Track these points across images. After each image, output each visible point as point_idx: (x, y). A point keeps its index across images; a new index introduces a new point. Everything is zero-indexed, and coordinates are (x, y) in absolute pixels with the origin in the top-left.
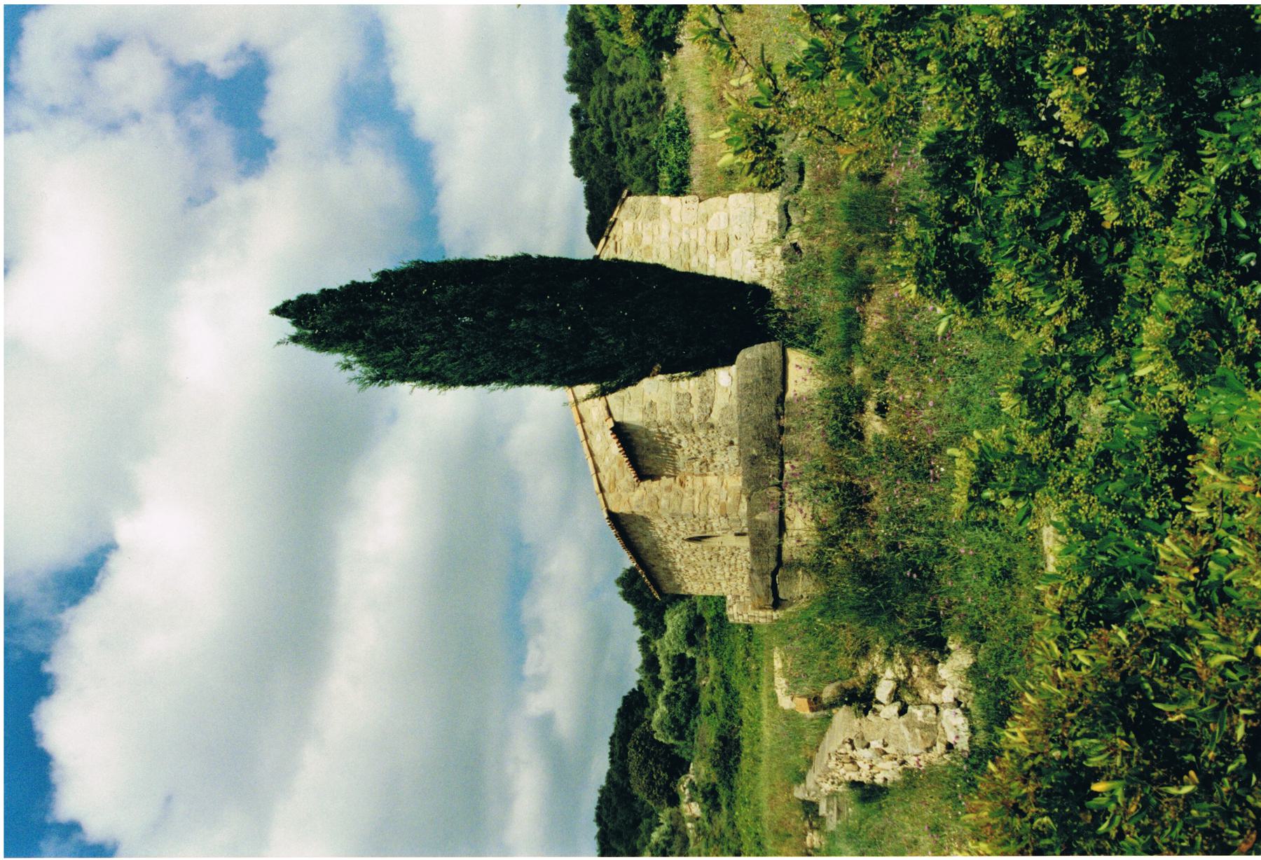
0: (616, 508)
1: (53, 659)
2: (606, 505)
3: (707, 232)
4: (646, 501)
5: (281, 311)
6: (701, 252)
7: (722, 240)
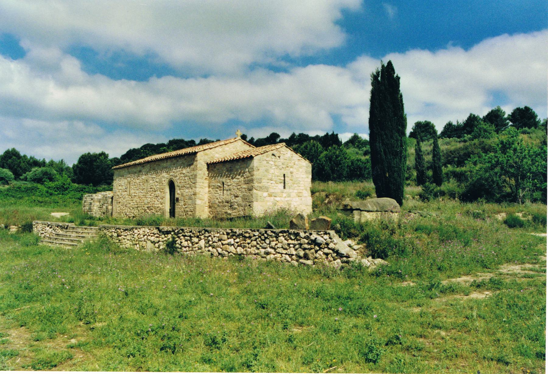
0: (198, 155)
2: (200, 151)
3: (303, 190)
6: (297, 188)
7: (301, 195)
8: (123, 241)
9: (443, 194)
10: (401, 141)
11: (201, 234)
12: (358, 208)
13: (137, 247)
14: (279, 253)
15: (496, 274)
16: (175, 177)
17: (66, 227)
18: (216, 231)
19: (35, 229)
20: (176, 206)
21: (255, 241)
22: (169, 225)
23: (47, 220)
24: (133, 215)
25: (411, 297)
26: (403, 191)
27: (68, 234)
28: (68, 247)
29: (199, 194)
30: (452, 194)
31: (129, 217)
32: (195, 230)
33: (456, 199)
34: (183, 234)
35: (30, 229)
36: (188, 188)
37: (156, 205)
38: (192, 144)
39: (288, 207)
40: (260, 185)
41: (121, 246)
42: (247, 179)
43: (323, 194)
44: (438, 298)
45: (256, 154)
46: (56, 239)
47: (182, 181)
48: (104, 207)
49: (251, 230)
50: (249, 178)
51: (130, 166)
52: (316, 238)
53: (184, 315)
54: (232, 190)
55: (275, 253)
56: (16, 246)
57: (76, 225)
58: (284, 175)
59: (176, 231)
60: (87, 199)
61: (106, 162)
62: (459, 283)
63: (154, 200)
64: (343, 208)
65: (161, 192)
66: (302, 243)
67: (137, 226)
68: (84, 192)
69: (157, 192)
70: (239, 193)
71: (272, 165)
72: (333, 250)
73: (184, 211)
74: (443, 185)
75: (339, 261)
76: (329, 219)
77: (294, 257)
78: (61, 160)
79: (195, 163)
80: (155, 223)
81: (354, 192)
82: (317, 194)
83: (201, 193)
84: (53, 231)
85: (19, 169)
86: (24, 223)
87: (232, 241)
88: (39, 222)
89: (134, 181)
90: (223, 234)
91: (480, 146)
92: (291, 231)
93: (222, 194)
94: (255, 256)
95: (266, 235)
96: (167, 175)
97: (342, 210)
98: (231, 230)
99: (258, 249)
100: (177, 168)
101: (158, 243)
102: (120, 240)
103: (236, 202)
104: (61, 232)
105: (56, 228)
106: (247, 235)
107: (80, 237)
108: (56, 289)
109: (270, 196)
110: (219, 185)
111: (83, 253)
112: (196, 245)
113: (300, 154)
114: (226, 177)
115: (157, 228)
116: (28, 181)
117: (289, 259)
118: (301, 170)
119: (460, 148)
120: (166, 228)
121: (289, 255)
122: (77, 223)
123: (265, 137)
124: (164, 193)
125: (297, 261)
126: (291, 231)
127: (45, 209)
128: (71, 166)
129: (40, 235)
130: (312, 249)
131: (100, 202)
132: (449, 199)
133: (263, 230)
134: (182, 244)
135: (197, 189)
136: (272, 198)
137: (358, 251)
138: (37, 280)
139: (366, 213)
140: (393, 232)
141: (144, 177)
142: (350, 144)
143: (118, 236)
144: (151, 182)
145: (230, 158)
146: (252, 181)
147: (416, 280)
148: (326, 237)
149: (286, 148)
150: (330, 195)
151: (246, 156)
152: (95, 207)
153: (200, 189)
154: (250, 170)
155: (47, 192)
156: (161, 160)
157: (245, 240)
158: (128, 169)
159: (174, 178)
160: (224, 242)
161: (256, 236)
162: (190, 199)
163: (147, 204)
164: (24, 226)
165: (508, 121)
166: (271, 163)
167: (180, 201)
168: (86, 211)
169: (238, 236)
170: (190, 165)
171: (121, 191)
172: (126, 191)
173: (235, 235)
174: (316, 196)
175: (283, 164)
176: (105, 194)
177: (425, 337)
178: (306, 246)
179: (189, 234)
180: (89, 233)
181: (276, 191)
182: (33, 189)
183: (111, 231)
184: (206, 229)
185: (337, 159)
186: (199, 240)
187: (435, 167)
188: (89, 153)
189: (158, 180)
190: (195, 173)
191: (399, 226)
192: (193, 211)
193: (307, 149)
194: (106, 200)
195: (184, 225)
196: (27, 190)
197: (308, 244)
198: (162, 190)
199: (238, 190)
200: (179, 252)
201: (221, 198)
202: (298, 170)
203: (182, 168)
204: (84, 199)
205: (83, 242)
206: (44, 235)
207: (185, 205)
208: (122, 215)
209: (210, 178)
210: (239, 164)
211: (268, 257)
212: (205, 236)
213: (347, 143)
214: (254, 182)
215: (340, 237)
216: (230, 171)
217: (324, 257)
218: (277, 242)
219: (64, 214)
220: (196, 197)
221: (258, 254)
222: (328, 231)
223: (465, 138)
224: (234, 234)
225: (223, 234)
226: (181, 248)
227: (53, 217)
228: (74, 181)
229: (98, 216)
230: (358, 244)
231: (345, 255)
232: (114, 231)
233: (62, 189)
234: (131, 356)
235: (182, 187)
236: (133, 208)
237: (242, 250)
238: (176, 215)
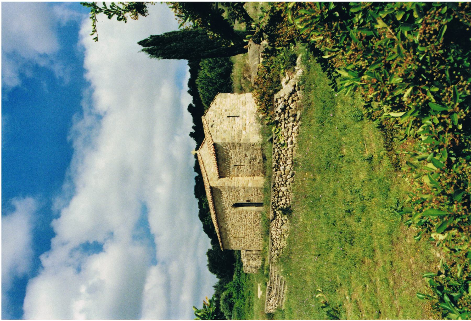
0: (212, 185)
1: (62, 217)
4: (221, 183)
6: (238, 105)
7: (244, 102)
8: (281, 246)
10: (202, 34)
14: (291, 134)
17: (270, 288)
19: (272, 311)
20: (254, 202)
22: (269, 212)
23: (265, 302)
24: (260, 235)
27: (275, 287)
28: (286, 288)
32: (273, 194)
36: (239, 193)
39: (254, 114)
40: (236, 137)
42: (232, 148)
46: (279, 296)
47: (233, 197)
48: (254, 256)
49: (273, 154)
50: (231, 146)
51: (221, 238)
52: (280, 109)
53: (333, 223)
54: (241, 158)
55: (291, 137)
57: (268, 281)
58: (228, 117)
59: (274, 208)
65: (242, 213)
67: (270, 236)
68: (241, 270)
70: (244, 152)
72: (289, 97)
73: (257, 195)
77: (294, 124)
78: (214, 288)
79: (219, 188)
80: (268, 223)
82: (243, 85)
87: (282, 168)
88: (266, 308)
89: (233, 234)
90: (276, 174)
94: (294, 151)
96: (229, 209)
98: (273, 168)
99: (288, 149)
100: (222, 202)
101: (283, 221)
102: (281, 248)
103: (250, 155)
105: (271, 295)
106: (277, 157)
107: (278, 278)
108: (316, 303)
109: (245, 129)
110: (236, 168)
111: (291, 278)
112: (285, 193)
117: (296, 127)
118: (224, 103)
120: (271, 215)
121: (293, 127)
122: (267, 280)
123: (191, 117)
125: (298, 122)
127: (255, 303)
128: (218, 280)
131: (249, 260)
133: (274, 146)
136: (247, 127)
137: (291, 77)
138: (310, 314)
141: (230, 227)
143: (277, 249)
144: (234, 221)
146: (233, 144)
148: (279, 101)
152: (254, 263)
153: (240, 184)
154: (225, 145)
155: (241, 299)
156: (216, 214)
157: (282, 158)
158: (223, 239)
159: (231, 204)
160: (283, 173)
162: (247, 191)
167: (249, 199)
168: (256, 271)
169: (278, 163)
170: (220, 191)
171: (241, 244)
174: (245, 86)
175: (219, 118)
176: (243, 255)
178: (286, 115)
179: (276, 198)
181: (241, 123)
182: (239, 311)
183: (273, 255)
184: (272, 186)
185: (212, 62)
186: (281, 191)
188: (208, 265)
189: (232, 216)
190: (227, 188)
192: (257, 189)
193: (204, 87)
194: (248, 255)
197: (285, 114)
198: (241, 213)
199: (241, 154)
200: (290, 206)
202: (224, 105)
204: (247, 272)
205: (282, 277)
208: (260, 243)
211: (294, 142)
212: (278, 187)
214: (234, 142)
215: (279, 90)
216: (225, 160)
217: (294, 103)
221: (292, 149)
222: (275, 100)
224: (276, 166)
225: (276, 174)
227: (262, 297)
231: (293, 88)
232: (273, 253)
233: (239, 287)
234: (356, 265)
237: (289, 160)
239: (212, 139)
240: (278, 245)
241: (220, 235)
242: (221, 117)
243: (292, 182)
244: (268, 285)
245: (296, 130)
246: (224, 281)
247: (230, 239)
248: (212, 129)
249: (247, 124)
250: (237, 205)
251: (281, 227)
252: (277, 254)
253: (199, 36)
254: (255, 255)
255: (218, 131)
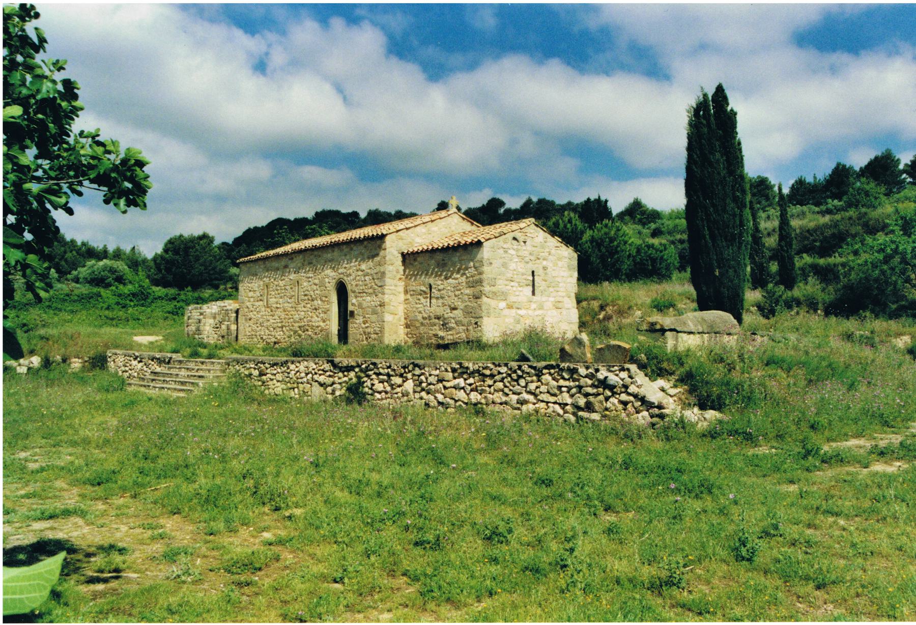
0: (388, 238)
3: (563, 297)
5: (720, 90)
7: (560, 305)
8: (270, 383)
9: (799, 303)
11: (407, 370)
12: (673, 327)
13: (294, 394)
14: (542, 401)
15: (907, 436)
16: (347, 276)
17: (167, 360)
18: (432, 365)
19: (111, 365)
20: (350, 325)
21: (500, 381)
23: (131, 349)
24: (274, 340)
25: (777, 469)
26: (742, 300)
27: (172, 371)
29: (389, 304)
30: (812, 303)
31: (268, 343)
32: (397, 364)
33: (819, 312)
34: (376, 370)
35: (103, 365)
36: (370, 294)
37: (314, 324)
38: (376, 218)
40: (493, 289)
41: (267, 392)
42: (471, 279)
43: (595, 305)
44: (819, 471)
45: (487, 238)
46: (153, 380)
47: (361, 283)
48: (224, 327)
49: (494, 364)
50: (474, 278)
51: (267, 258)
52: (606, 378)
54: (447, 298)
55: (535, 401)
56: (89, 391)
57: (184, 356)
58: (533, 272)
59: (363, 366)
60: (193, 314)
61: (211, 250)
62: (850, 449)
63: (310, 314)
64: (648, 328)
66: (581, 384)
69: (315, 301)
70: (459, 304)
71: (512, 255)
72: (635, 396)
74: (796, 288)
75: (645, 413)
76: (627, 346)
77: (568, 408)
79: (382, 253)
80: (323, 353)
81: (648, 301)
82: (584, 304)
83: (392, 304)
84: (145, 367)
85: (63, 263)
86: (92, 353)
87: (461, 382)
88: (118, 352)
90: (446, 370)
91: (861, 222)
92: (562, 365)
93: (428, 304)
95: (519, 372)
96: (334, 273)
97: (647, 331)
98: (460, 364)
99: (507, 395)
101: (331, 385)
102: (264, 382)
103: (454, 318)
104: (158, 369)
105: (150, 362)
106: (488, 372)
107: (195, 376)
109: (510, 307)
110: (424, 289)
112: (399, 390)
113: (559, 237)
114: (436, 276)
115: (328, 362)
116: (80, 283)
118: (560, 264)
119: (825, 226)
121: (560, 404)
122: (185, 354)
123: (479, 205)
124: (329, 302)
125: (574, 414)
126: (562, 365)
129: (120, 373)
130: (599, 394)
131: (215, 318)
132: (808, 312)
133: (514, 365)
134: (374, 388)
135: (386, 296)
136: (513, 311)
139: (684, 336)
140: (731, 368)
141: (292, 276)
142: (627, 218)
143: (262, 374)
144: (305, 284)
145: (441, 245)
146: (480, 282)
147: (775, 444)
148: (624, 375)
149: (536, 228)
150: (607, 305)
151: (470, 241)
154: (477, 265)
156: (323, 248)
157: (484, 381)
158: (264, 263)
159: (345, 278)
160: (448, 384)
161: (502, 373)
162: (374, 312)
163: (298, 322)
164: (93, 359)
165: (904, 176)
166: (511, 252)
167: (356, 317)
168: (191, 333)
169: (472, 374)
170: (373, 257)
171: (252, 300)
172: (261, 300)
173: (467, 372)
175: (530, 254)
177: (815, 527)
178: (590, 390)
179: (386, 371)
180: (209, 371)
181: (520, 299)
182: (92, 297)
183: (248, 366)
184: (417, 362)
186: (404, 381)
187: (782, 255)
188: (181, 236)
189: (317, 281)
191: (741, 357)
195: (375, 356)
196: (81, 299)
197: (593, 386)
198: (324, 298)
199: (456, 298)
201: (427, 311)
202: (555, 265)
203: (360, 262)
205: (201, 385)
206: (127, 374)
207: (365, 324)
208: (256, 340)
209: (406, 278)
210: (458, 254)
211: (524, 408)
212: (414, 375)
213: (621, 215)
214: (484, 284)
215: (646, 375)
216: (442, 265)
217: (620, 407)
218: (539, 383)
219: (157, 338)
220: (384, 310)
221: (506, 403)
222: (627, 366)
223: (830, 206)
224: (465, 370)
225: (446, 370)
226: (372, 395)
228: (156, 283)
229: (212, 342)
230: (675, 386)
231: (656, 404)
232: (253, 366)
233: (141, 297)
235: (360, 293)
236: (274, 329)
237: (479, 397)
238: (350, 340)
239: (489, 239)
240: (272, 377)
241: (272, 257)
242: (532, 258)
243: (427, 405)
244: (174, 356)
245: (554, 412)
246: (149, 268)
247: (265, 277)
248: (511, 238)
249: (519, 312)
250: (342, 291)
251: (316, 381)
252: (251, 375)
253: (737, 211)
254: (228, 329)
255: (506, 252)
